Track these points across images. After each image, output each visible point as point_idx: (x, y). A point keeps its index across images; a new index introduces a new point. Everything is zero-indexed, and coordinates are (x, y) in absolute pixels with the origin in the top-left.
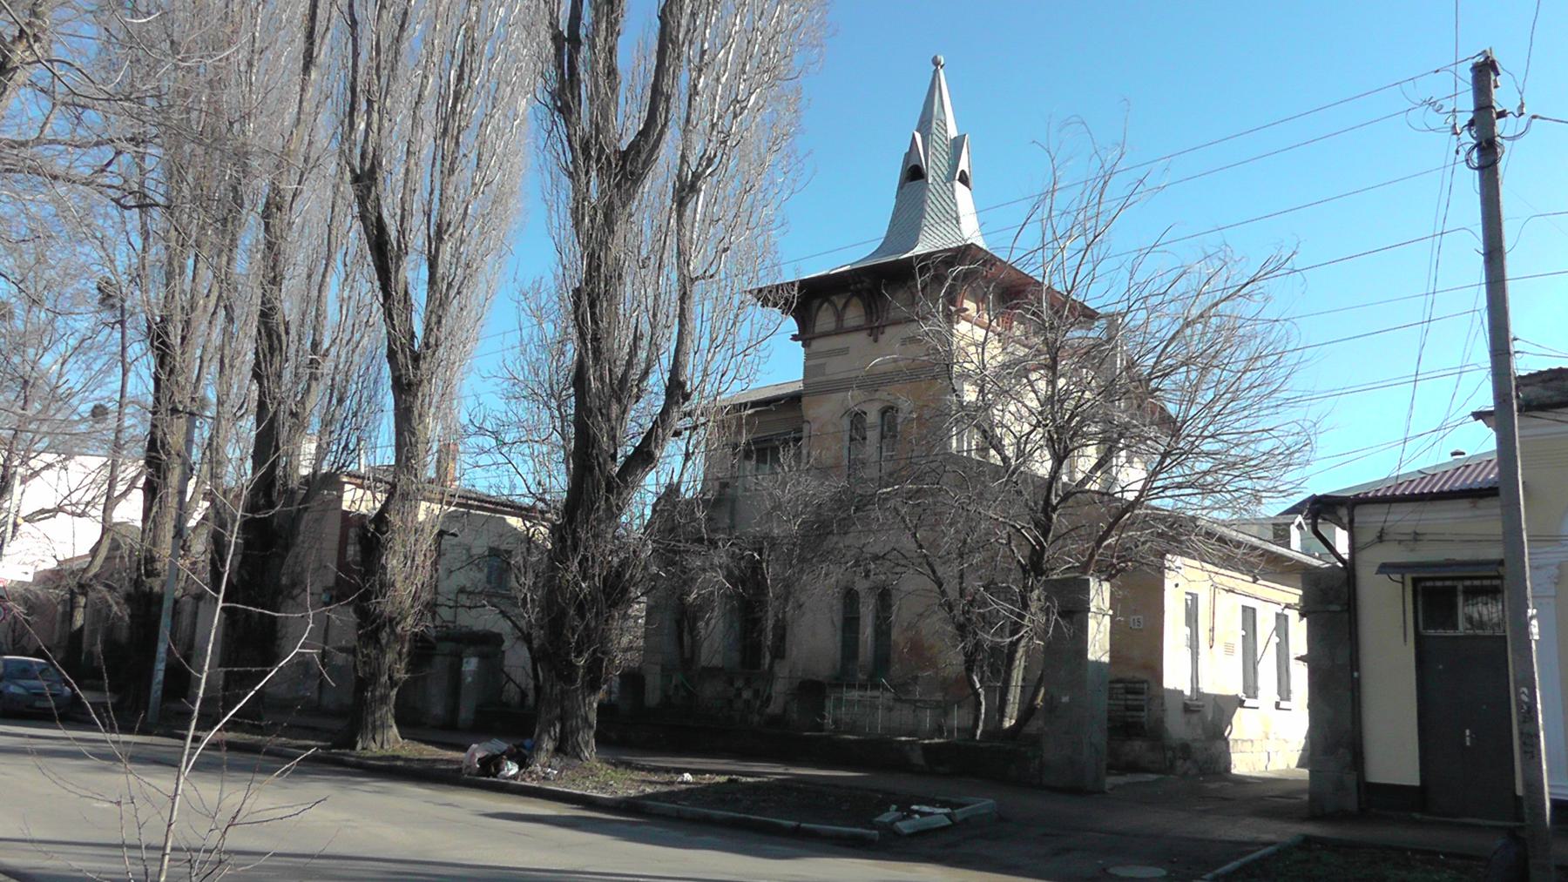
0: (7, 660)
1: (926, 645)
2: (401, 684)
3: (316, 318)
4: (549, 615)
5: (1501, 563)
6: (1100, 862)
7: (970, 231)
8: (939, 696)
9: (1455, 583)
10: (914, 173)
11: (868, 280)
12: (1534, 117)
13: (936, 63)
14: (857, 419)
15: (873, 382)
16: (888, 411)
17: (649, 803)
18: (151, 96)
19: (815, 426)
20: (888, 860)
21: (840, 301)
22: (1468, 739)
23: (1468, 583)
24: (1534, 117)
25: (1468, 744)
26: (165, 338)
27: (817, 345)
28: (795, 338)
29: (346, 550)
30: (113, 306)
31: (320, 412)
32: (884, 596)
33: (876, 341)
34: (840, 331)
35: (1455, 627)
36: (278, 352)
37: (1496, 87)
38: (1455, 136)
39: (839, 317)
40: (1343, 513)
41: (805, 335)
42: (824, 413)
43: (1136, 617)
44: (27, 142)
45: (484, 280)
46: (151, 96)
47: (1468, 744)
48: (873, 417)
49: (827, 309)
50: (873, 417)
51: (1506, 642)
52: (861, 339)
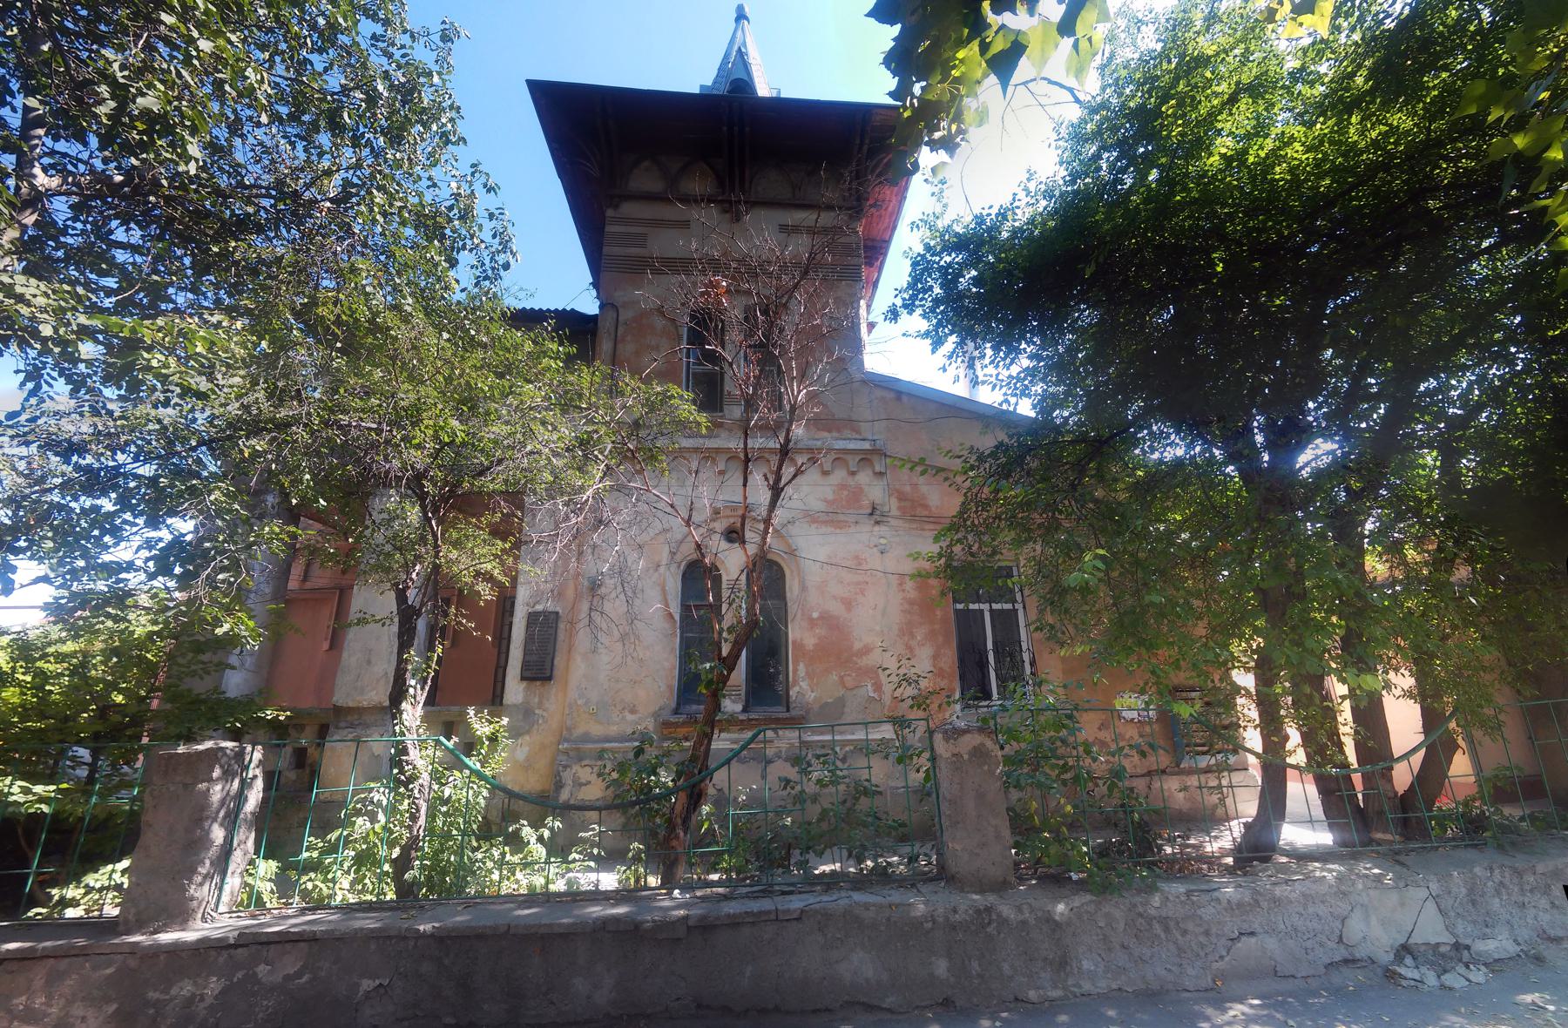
0: (27, 879)
1: (857, 646)
2: (1486, 162)
3: (917, 1007)
4: (1168, 436)
5: (501, 704)
6: (1369, 526)
8: (402, 790)
13: (741, 16)
18: (777, 491)
20: (818, 102)
26: (1019, 606)
29: (1266, 738)
30: (794, 805)
31: (590, 869)
33: (867, 15)
36: (232, 793)
44: (334, 628)
45: (387, 604)
46: (777, 491)
51: (525, 665)
52: (705, 216)
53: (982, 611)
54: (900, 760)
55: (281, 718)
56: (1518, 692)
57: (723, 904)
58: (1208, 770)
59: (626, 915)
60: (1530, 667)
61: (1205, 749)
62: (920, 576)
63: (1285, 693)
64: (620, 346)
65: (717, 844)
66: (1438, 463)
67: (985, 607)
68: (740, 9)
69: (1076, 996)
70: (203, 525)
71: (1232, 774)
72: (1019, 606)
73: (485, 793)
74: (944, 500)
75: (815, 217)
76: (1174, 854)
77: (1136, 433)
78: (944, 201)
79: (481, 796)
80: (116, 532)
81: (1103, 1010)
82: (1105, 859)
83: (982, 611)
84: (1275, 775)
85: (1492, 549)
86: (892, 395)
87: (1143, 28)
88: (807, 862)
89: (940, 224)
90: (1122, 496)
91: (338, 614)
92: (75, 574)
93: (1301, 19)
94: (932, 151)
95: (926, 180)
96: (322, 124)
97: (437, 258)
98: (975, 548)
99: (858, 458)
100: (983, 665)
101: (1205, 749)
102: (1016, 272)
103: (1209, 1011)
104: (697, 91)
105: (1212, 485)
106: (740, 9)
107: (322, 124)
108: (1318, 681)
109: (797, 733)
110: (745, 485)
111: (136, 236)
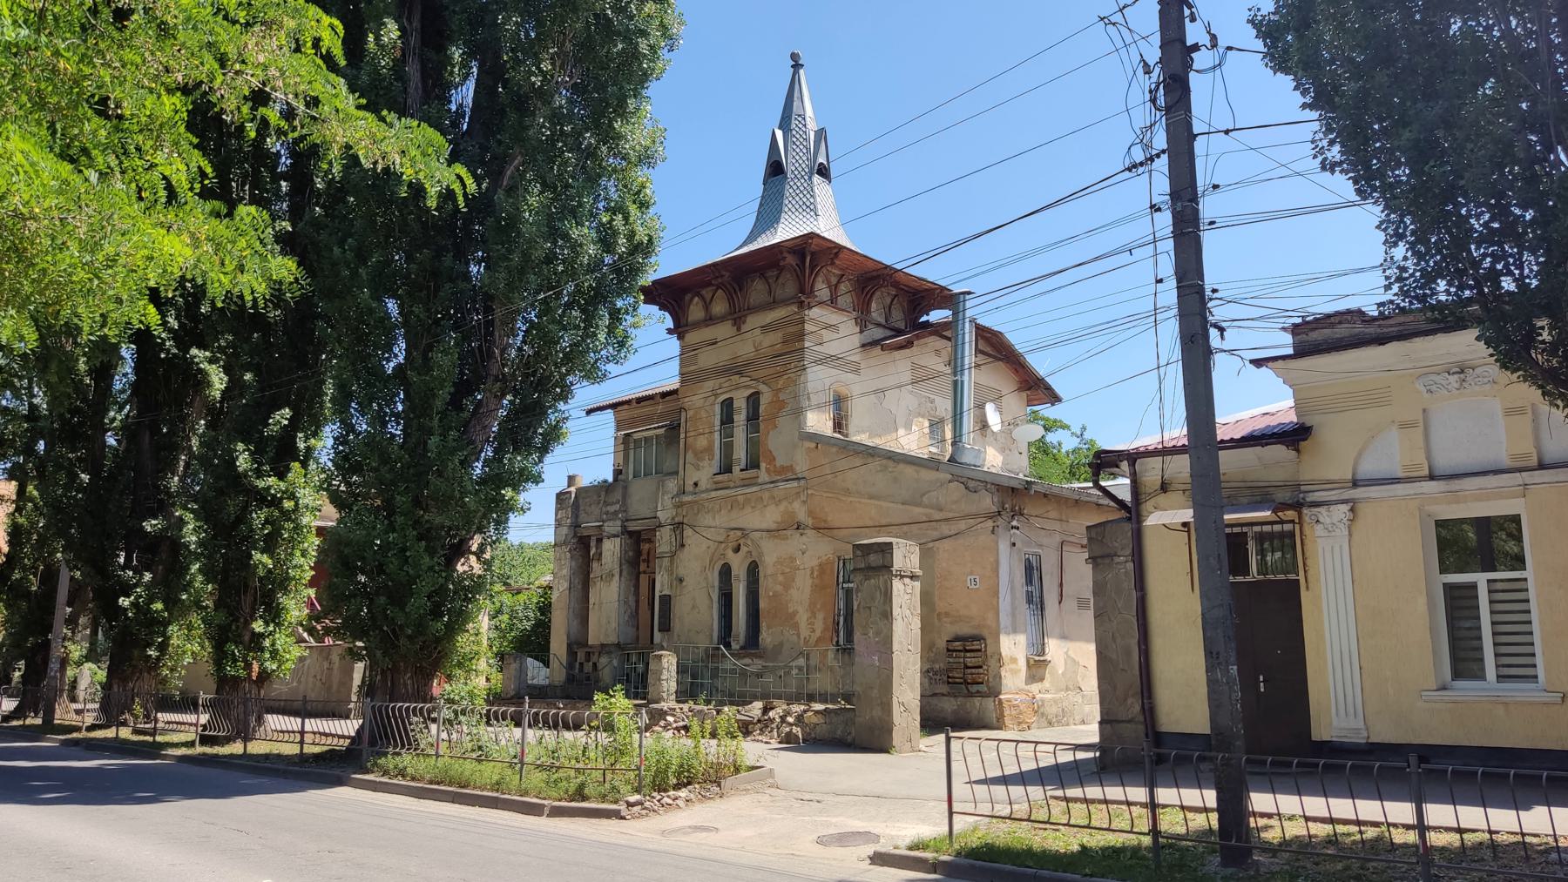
7: (829, 227)
9: (1245, 529)
10: (775, 169)
11: (727, 274)
12: (1229, 48)
14: (728, 405)
15: (735, 369)
16: (754, 400)
17: (15, 723)
19: (690, 413)
21: (707, 293)
22: (1262, 684)
23: (1257, 529)
24: (1229, 48)
25: (1262, 690)
27: (693, 337)
28: (670, 331)
32: (753, 570)
34: (710, 320)
35: (1246, 572)
37: (1193, 20)
38: (1147, 76)
39: (707, 307)
40: (1125, 465)
42: (703, 406)
43: (972, 577)
47: (1262, 690)
48: (740, 403)
49: (697, 303)
50: (740, 403)
52: (724, 330)
53: (1473, 587)
54: (948, 650)
55: (288, 162)
56: (678, 526)
58: (172, 723)
59: (355, 773)
60: (59, 555)
62: (1146, 471)
67: (1481, 579)
68: (794, 57)
70: (364, 178)
71: (120, 728)
72: (1301, 578)
73: (170, 628)
75: (960, 823)
76: (465, 572)
82: (66, 168)
83: (1473, 587)
88: (378, 104)
89: (648, 184)
90: (319, 627)
91: (696, 827)
92: (325, 419)
93: (744, 328)
98: (790, 719)
99: (760, 481)
100: (1362, 767)
102: (188, 285)
103: (158, 331)
104: (635, 135)
106: (794, 57)
108: (441, 49)
109: (305, 751)
110: (1060, 603)
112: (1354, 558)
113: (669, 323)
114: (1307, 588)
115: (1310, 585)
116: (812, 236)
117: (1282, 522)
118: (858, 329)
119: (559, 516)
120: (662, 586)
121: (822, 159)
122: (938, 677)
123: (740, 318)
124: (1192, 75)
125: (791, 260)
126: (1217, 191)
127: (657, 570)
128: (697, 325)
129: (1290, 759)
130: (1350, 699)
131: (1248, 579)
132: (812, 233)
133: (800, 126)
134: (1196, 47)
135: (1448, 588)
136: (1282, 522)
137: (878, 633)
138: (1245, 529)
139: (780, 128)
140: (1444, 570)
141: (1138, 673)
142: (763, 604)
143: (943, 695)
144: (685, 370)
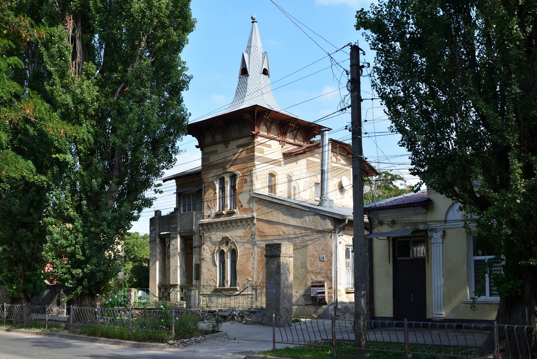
9: (409, 239)
34: (214, 143)
41: (201, 146)
52: (220, 147)
57: (247, 142)
61: (227, 179)
63: (129, 157)
64: (488, 305)
65: (195, 220)
66: (521, 94)
69: (17, 180)
74: (334, 205)
77: (410, 36)
78: (364, 37)
79: (318, 276)
80: (50, 90)
81: (43, 297)
84: (223, 198)
85: (338, 348)
86: (259, 199)
87: (255, 248)
89: (437, 236)
94: (181, 52)
95: (364, 54)
96: (137, 264)
97: (66, 276)
101: (227, 179)
105: (178, 48)
107: (137, 264)
111: (187, 340)
112: (444, 251)
113: (197, 143)
114: (428, 262)
115: (429, 261)
116: (256, 106)
117: (416, 237)
118: (281, 146)
119: (151, 229)
120: (196, 260)
121: (265, 66)
122: (308, 298)
123: (227, 141)
124: (361, 77)
125: (248, 116)
126: (366, 123)
127: (194, 253)
128: (209, 145)
129: (412, 322)
130: (439, 303)
131: (409, 258)
132: (256, 105)
133: (255, 51)
134: (363, 67)
135: (476, 261)
136: (416, 237)
137: (275, 280)
138: (409, 239)
139: (247, 52)
140: (476, 254)
141: (238, 277)
142: (238, 268)
143: (310, 305)
144: (204, 164)
